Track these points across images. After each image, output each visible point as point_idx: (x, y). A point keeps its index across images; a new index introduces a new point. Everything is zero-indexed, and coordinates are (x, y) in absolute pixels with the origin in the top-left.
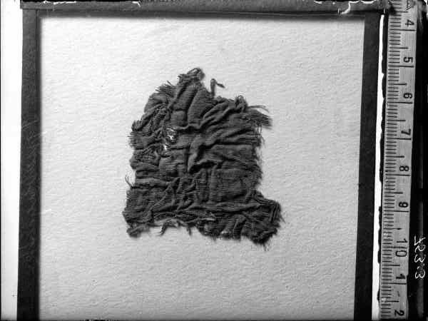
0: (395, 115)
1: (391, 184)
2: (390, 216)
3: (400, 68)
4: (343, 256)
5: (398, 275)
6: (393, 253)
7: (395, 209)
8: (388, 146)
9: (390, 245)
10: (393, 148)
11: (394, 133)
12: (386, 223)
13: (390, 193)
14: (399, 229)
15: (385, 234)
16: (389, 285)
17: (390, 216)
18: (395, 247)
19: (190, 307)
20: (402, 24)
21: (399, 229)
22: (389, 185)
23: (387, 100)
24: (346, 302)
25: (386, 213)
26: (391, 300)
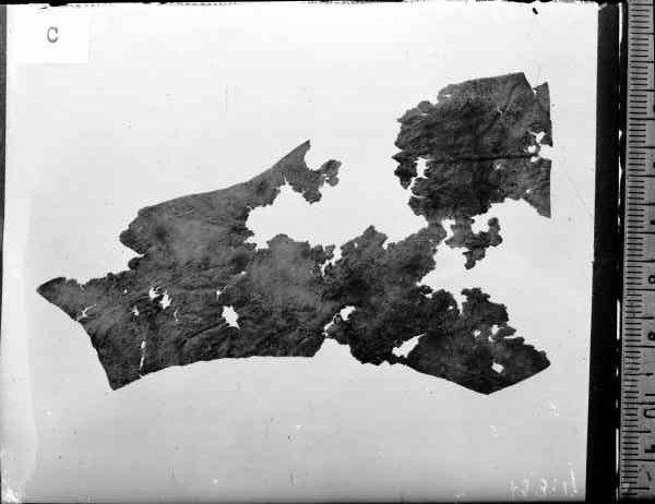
0: (642, 139)
1: (635, 304)
2: (635, 355)
3: (647, 122)
4: (456, 138)
5: (649, 448)
6: (640, 412)
7: (642, 343)
8: (631, 142)
9: (635, 401)
10: (638, 247)
11: (635, 452)
12: (627, 366)
13: (635, 204)
14: (648, 374)
15: (626, 383)
16: (639, 207)
17: (635, 355)
18: (643, 403)
19: (294, 310)
20: (646, 168)
21: (648, 374)
22: (632, 306)
23: (628, 173)
24: (575, 480)
25: (633, 99)
26: (637, 486)
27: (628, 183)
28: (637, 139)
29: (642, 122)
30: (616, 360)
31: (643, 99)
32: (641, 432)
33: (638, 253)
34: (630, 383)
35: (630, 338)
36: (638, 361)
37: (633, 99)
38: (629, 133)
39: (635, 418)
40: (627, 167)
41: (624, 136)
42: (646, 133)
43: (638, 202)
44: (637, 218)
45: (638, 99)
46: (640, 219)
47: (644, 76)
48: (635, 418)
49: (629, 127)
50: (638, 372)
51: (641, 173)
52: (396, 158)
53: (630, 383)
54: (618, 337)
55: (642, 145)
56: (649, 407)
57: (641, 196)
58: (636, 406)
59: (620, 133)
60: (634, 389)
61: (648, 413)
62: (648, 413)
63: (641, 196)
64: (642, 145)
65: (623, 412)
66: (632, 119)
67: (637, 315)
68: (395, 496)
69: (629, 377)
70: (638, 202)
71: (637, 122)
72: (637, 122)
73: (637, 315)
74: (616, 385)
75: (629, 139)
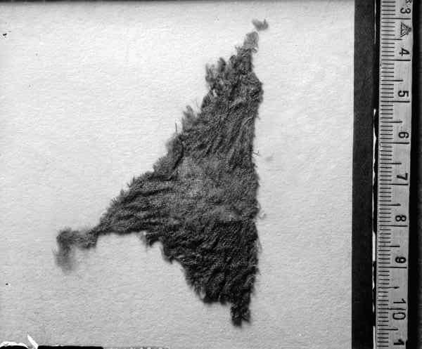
2: (385, 273)
5: (397, 341)
14: (396, 288)
15: (380, 294)
17: (385, 273)
20: (391, 261)
23: (380, 141)
27: (380, 148)
28: (386, 136)
29: (390, 104)
30: (371, 320)
31: (391, 87)
32: (391, 246)
33: (387, 199)
34: (382, 294)
35: (382, 261)
36: (388, 278)
37: (382, 219)
38: (380, 112)
39: (386, 319)
40: (380, 136)
41: (377, 112)
42: (391, 195)
43: (386, 224)
44: (387, 132)
45: (387, 87)
46: (389, 174)
47: (392, 50)
48: (386, 319)
49: (381, 107)
50: (388, 286)
51: (390, 161)
52: (185, 113)
53: (382, 294)
54: (374, 259)
55: (390, 120)
56: (396, 311)
57: (390, 157)
58: (387, 311)
59: (375, 111)
60: (385, 298)
61: (396, 316)
62: (396, 316)
63: (390, 157)
64: (390, 120)
65: (378, 315)
66: (381, 188)
67: (387, 244)
68: (153, 3)
69: (381, 290)
70: (386, 224)
71: (386, 104)
72: (386, 104)
73: (387, 244)
74: (374, 78)
75: (380, 116)
